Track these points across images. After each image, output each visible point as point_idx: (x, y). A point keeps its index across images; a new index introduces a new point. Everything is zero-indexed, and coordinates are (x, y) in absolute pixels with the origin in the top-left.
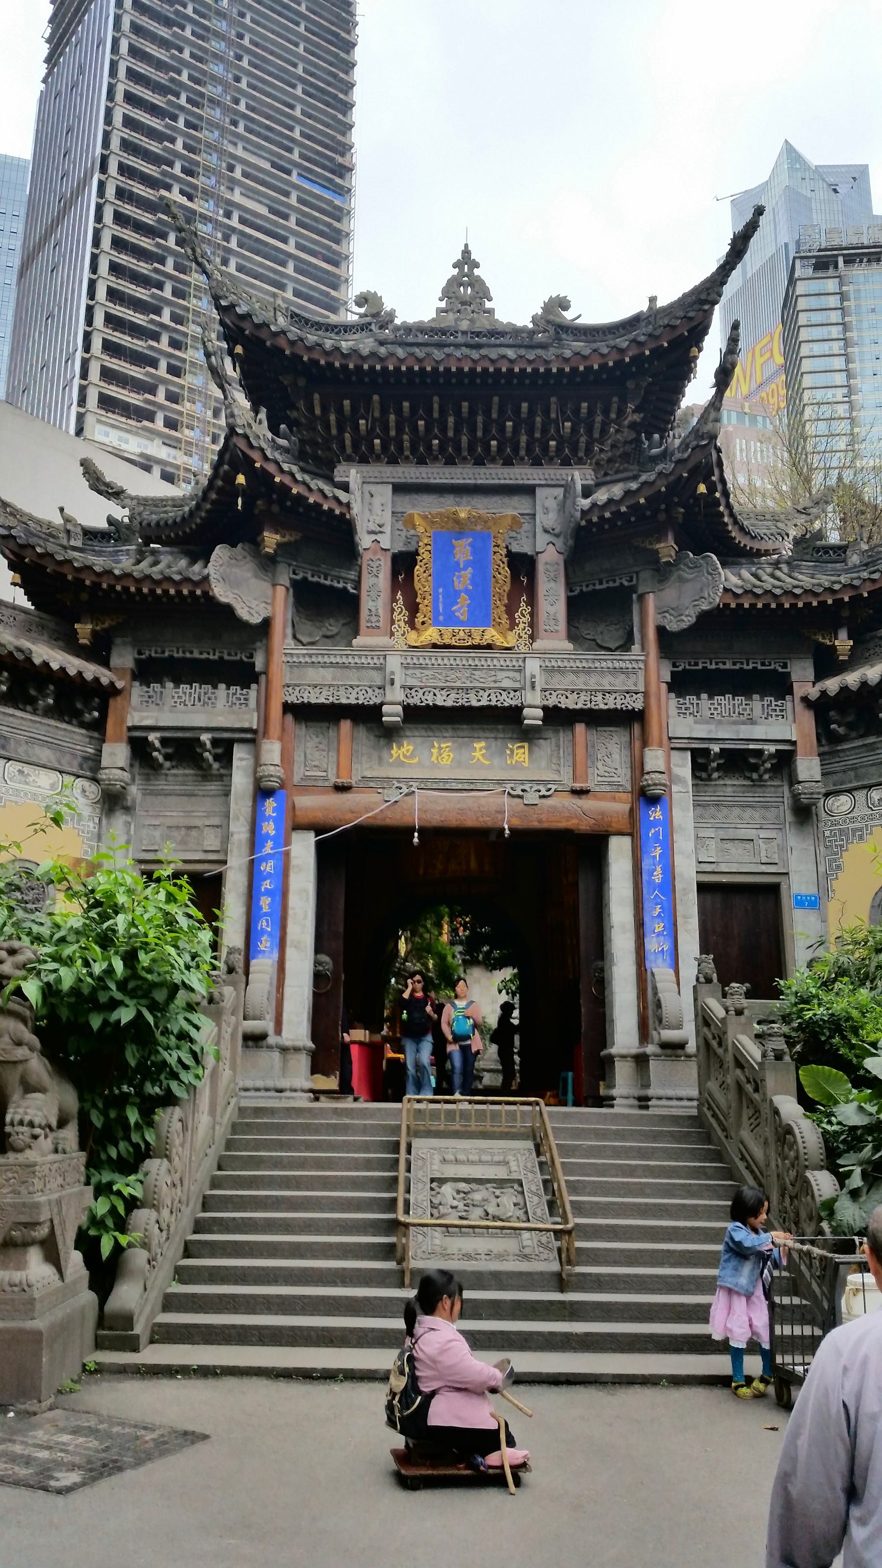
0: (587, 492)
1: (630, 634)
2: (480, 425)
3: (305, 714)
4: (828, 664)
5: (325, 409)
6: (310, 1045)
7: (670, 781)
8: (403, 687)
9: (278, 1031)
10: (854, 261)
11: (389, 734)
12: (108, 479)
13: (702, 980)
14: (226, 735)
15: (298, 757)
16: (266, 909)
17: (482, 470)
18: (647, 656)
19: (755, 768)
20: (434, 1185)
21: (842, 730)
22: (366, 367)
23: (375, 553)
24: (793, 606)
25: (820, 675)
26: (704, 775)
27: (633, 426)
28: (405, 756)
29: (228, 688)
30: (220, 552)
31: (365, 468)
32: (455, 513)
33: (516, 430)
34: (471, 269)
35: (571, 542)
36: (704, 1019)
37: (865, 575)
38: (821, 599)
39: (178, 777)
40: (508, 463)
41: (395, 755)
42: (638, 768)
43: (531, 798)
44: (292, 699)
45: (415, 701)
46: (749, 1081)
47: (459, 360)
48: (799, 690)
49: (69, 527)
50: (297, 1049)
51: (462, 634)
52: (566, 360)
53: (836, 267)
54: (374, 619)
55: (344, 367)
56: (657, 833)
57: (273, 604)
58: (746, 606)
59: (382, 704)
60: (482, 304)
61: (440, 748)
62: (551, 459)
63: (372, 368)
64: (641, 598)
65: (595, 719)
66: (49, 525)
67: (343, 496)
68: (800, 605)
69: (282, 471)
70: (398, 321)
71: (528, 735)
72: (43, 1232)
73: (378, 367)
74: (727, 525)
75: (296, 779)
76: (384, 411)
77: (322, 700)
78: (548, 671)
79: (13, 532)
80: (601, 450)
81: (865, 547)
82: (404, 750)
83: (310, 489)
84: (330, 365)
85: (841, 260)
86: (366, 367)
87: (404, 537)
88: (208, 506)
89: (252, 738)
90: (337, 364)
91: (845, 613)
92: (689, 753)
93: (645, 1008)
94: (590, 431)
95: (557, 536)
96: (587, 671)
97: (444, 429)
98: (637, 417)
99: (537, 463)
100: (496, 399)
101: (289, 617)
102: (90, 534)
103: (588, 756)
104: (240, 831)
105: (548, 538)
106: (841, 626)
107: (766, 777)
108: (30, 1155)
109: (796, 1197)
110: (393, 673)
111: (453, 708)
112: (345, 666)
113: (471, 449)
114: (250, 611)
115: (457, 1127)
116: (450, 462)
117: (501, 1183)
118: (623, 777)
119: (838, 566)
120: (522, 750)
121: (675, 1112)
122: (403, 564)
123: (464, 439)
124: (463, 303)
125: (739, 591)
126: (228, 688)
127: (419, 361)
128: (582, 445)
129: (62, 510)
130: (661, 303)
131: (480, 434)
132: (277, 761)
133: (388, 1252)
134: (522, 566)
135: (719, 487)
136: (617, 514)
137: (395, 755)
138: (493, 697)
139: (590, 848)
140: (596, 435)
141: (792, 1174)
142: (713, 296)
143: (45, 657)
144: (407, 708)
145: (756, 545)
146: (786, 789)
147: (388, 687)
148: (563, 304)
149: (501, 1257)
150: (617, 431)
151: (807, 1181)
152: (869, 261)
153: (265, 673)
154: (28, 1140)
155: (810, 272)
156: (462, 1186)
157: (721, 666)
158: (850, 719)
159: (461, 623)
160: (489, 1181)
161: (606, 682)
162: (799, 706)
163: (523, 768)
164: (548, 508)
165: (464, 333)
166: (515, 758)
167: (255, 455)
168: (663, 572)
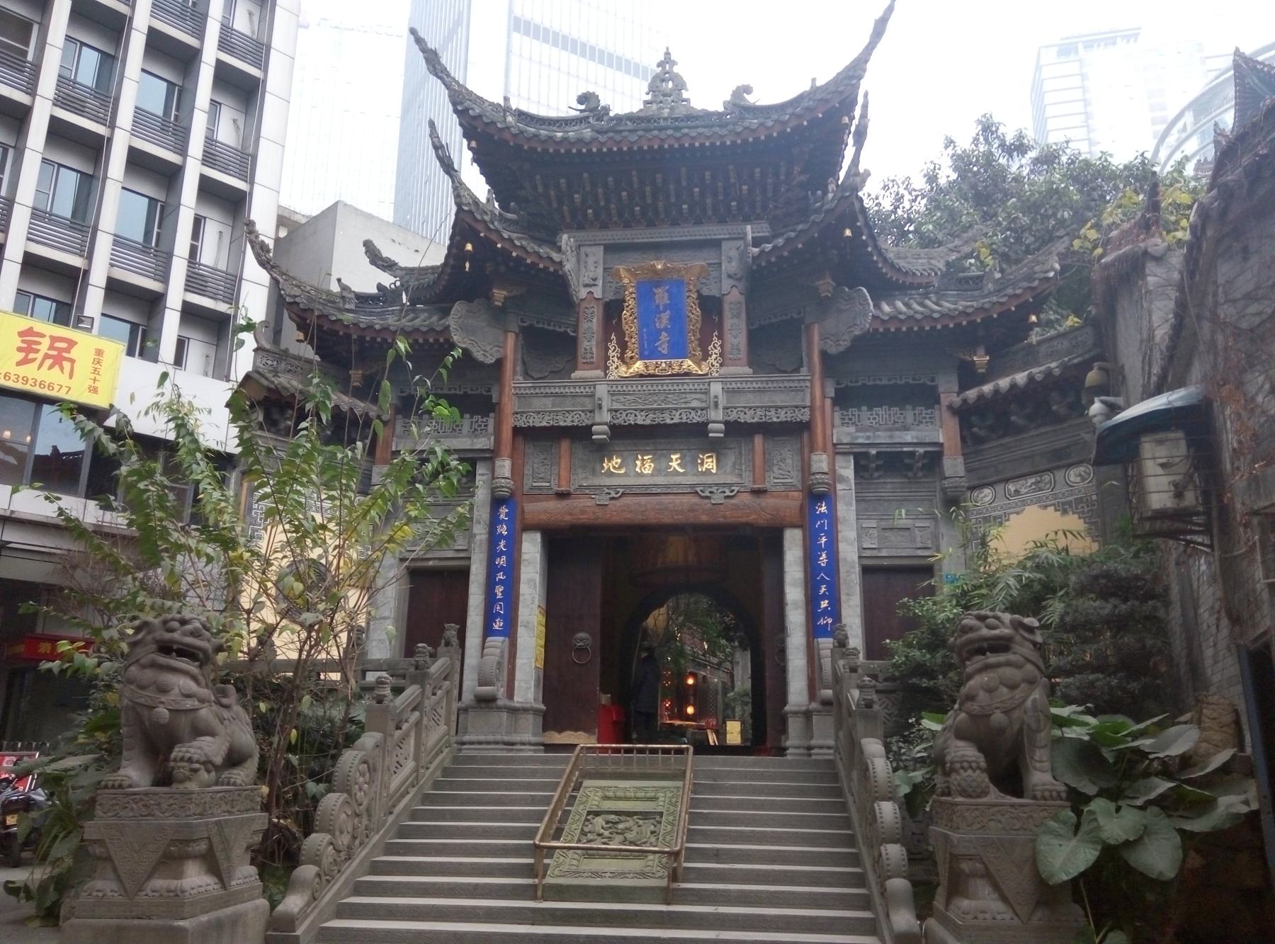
0: (757, 242)
3: (524, 434)
4: (969, 377)
6: (543, 707)
8: (610, 410)
9: (510, 695)
10: (1092, 46)
11: (602, 450)
12: (384, 255)
14: (470, 455)
15: (528, 471)
16: (499, 596)
17: (678, 230)
18: (813, 376)
19: (910, 467)
22: (574, 151)
25: (964, 387)
26: (866, 475)
30: (458, 308)
32: (653, 266)
33: (702, 194)
34: (671, 67)
38: (957, 321)
40: (698, 222)
42: (806, 469)
43: (718, 498)
44: (521, 424)
45: (620, 421)
47: (650, 140)
48: (945, 400)
49: (345, 294)
50: (525, 710)
52: (738, 134)
53: (1077, 52)
54: (588, 356)
57: (504, 347)
60: (680, 94)
63: (579, 151)
64: (808, 327)
65: (771, 431)
68: (939, 327)
69: (503, 238)
71: (715, 447)
72: (203, 847)
73: (584, 150)
75: (526, 488)
77: (544, 424)
78: (726, 391)
79: (297, 300)
80: (776, 207)
81: (998, 275)
84: (545, 151)
85: (1080, 46)
86: (574, 151)
89: (490, 456)
90: (551, 150)
92: (852, 458)
95: (739, 280)
96: (761, 391)
97: (643, 197)
99: (722, 221)
101: (519, 357)
102: (363, 299)
103: (765, 461)
104: (480, 532)
105: (732, 282)
108: (192, 786)
111: (651, 426)
114: (485, 354)
115: (622, 769)
117: (645, 815)
118: (795, 479)
119: (976, 293)
122: (613, 310)
124: (664, 95)
127: (618, 143)
130: (818, 84)
131: (673, 199)
132: (508, 474)
133: (529, 871)
134: (711, 307)
138: (684, 417)
140: (770, 195)
142: (859, 72)
144: (613, 427)
148: (747, 89)
149: (623, 875)
152: (1106, 45)
153: (499, 404)
154: (187, 773)
156: (612, 817)
157: (878, 382)
158: (989, 423)
160: (635, 813)
161: (779, 399)
162: (946, 415)
164: (731, 260)
165: (665, 119)
167: (480, 227)
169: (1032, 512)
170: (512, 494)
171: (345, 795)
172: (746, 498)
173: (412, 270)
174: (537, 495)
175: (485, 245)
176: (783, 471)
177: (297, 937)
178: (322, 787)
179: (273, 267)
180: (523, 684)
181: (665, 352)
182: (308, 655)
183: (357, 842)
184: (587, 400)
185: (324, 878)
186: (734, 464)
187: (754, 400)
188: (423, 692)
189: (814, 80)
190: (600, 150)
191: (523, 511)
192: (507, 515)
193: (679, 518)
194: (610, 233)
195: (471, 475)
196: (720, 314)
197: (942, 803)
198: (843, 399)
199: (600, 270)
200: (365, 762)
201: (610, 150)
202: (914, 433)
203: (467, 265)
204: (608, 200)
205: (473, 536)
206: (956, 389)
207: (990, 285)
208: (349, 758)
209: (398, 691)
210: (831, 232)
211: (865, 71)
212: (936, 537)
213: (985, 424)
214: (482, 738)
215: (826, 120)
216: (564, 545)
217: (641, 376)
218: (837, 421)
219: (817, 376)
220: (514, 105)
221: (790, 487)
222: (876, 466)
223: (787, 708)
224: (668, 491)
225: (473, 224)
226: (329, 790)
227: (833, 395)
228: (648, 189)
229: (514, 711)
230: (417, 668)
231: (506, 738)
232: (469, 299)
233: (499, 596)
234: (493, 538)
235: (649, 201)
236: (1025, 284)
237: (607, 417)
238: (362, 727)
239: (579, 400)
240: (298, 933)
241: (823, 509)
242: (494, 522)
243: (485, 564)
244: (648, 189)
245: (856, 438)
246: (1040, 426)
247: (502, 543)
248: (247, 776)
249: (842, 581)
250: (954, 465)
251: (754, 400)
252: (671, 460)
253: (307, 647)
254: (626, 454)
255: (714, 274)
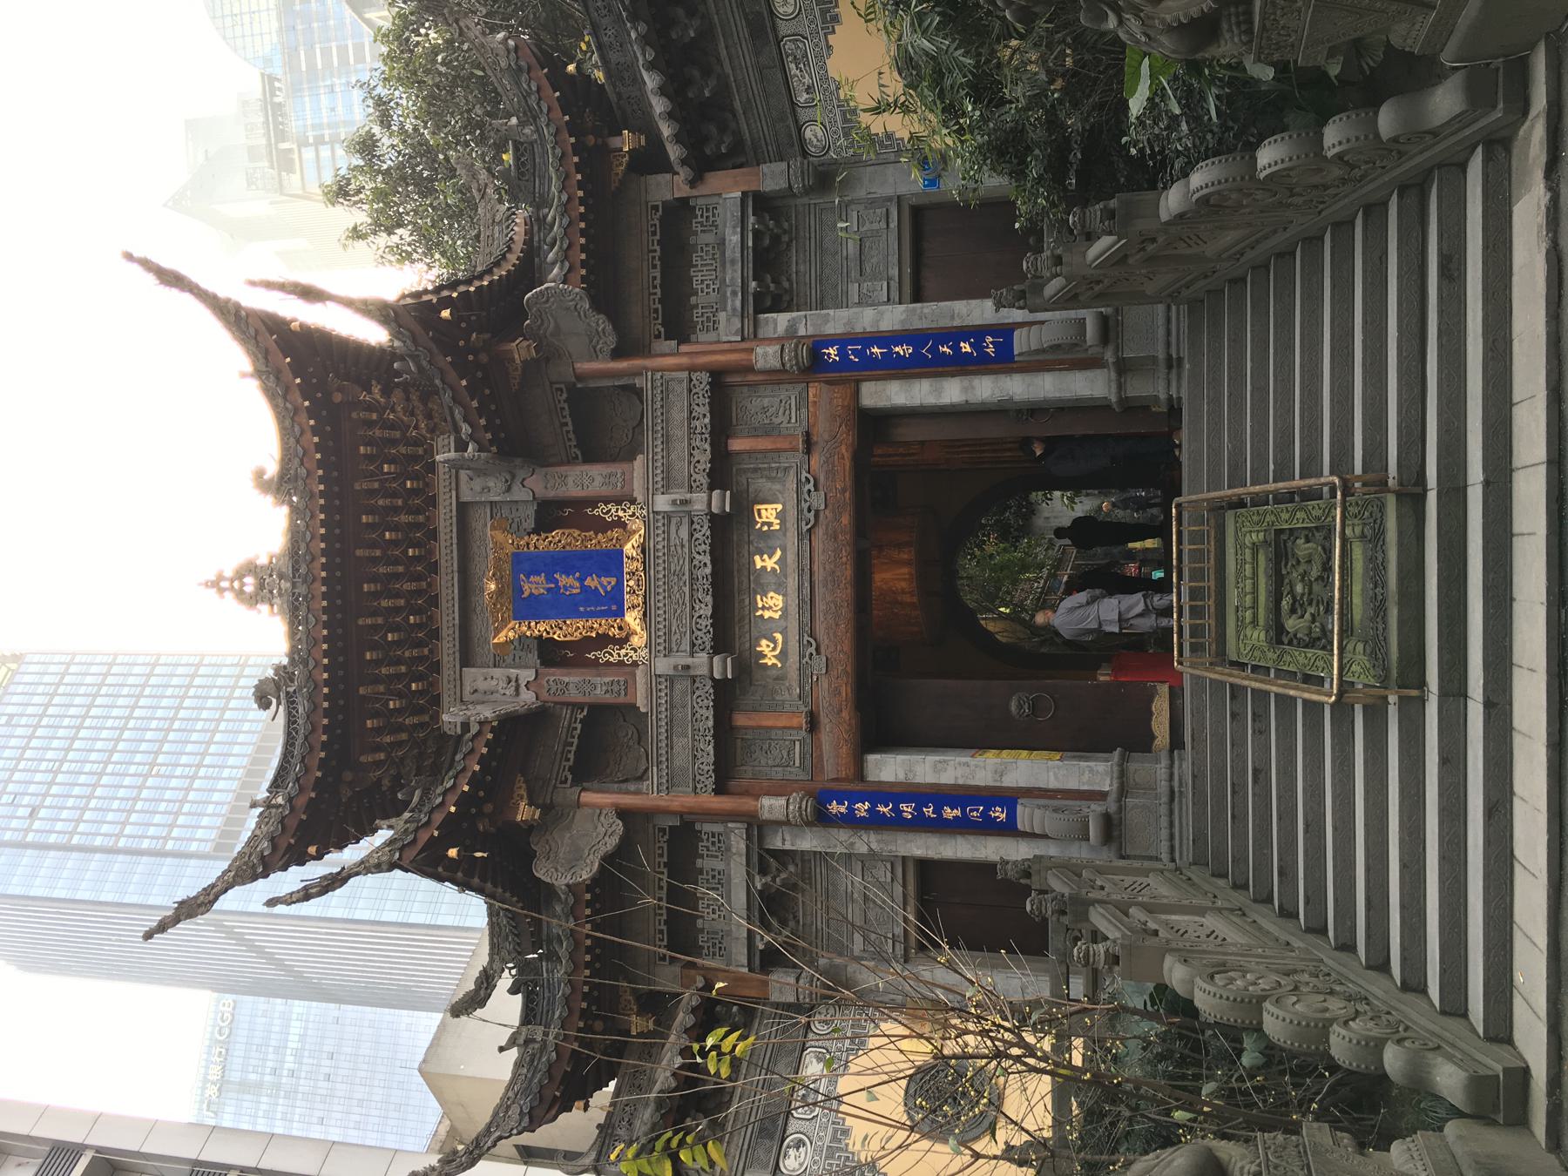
0: (461, 446)
1: (623, 387)
2: (390, 569)
5: (378, 748)
6: (1117, 753)
7: (792, 338)
9: (1102, 796)
10: (283, 131)
11: (747, 666)
13: (1022, 303)
15: (778, 773)
16: (957, 812)
18: (647, 369)
19: (776, 239)
20: (1286, 640)
21: (728, 139)
23: (542, 686)
24: (582, 201)
26: (786, 298)
27: (386, 392)
28: (774, 649)
29: (702, 856)
30: (542, 872)
31: (445, 699)
33: (395, 528)
35: (518, 461)
36: (1069, 300)
37: (543, 120)
39: (809, 906)
40: (433, 535)
41: (774, 661)
42: (777, 377)
43: (818, 501)
44: (710, 783)
45: (708, 639)
46: (1143, 249)
48: (683, 190)
49: (521, 1041)
50: (1122, 774)
51: (631, 583)
55: (326, 729)
56: (854, 352)
58: (583, 256)
59: (713, 679)
61: (763, 608)
62: (427, 485)
63: (326, 697)
64: (580, 377)
65: (721, 429)
66: (518, 1064)
67: (474, 729)
68: (580, 193)
69: (442, 804)
70: (285, 661)
71: (743, 510)
73: (326, 690)
74: (491, 282)
76: (377, 680)
77: (710, 749)
80: (416, 427)
81: (514, 120)
82: (767, 651)
83: (464, 769)
87: (523, 654)
88: (489, 885)
89: (757, 828)
91: (591, 140)
93: (1061, 362)
94: (394, 442)
95: (513, 477)
96: (667, 440)
97: (397, 610)
98: (376, 390)
99: (432, 502)
100: (359, 553)
102: (528, 1016)
104: (867, 842)
105: (516, 487)
106: (606, 144)
107: (786, 225)
109: (1291, 190)
110: (675, 668)
112: (670, 723)
113: (418, 578)
114: (608, 835)
116: (434, 601)
118: (790, 394)
120: (763, 513)
121: (1185, 325)
122: (551, 653)
123: (407, 586)
125: (567, 264)
126: (702, 856)
128: (410, 450)
129: (501, 1049)
132: (782, 801)
134: (550, 515)
135: (445, 293)
136: (480, 411)
137: (774, 661)
139: (874, 427)
141: (1259, 195)
143: (668, 1074)
144: (716, 650)
145: (518, 246)
146: (799, 201)
147: (692, 673)
148: (259, 474)
150: (393, 410)
151: (1270, 177)
153: (681, 814)
155: (295, 178)
156: (1285, 604)
157: (658, 282)
159: (620, 583)
161: (679, 415)
163: (783, 510)
164: (483, 489)
165: (294, 585)
166: (772, 519)
167: (424, 837)
168: (548, 354)
169: (837, 67)
170: (809, 794)
171: (1267, 1005)
172: (816, 460)
173: (492, 945)
174: (813, 762)
175: (452, 830)
176: (782, 411)
177: (1505, 1070)
178: (1248, 1042)
179: (478, 1146)
180: (1087, 776)
181: (613, 581)
182: (1045, 1058)
183: (1338, 988)
184: (678, 687)
185: (1402, 1034)
186: (769, 478)
187: (680, 448)
188: (1101, 902)
189: (244, 375)
190: (326, 668)
191: (833, 780)
192: (840, 803)
193: (846, 555)
194: (446, 659)
195: (783, 856)
196: (562, 503)
197: (1263, 28)
198: (679, 327)
199: (497, 672)
200: (1212, 977)
201: (326, 654)
202: (728, 231)
203: (478, 854)
204: (399, 662)
205: (872, 854)
206: (668, 176)
207: (527, 131)
208: (1207, 1000)
209: (1096, 937)
210: (444, 337)
211: (228, 301)
212: (872, 203)
213: (712, 137)
214: (1164, 834)
215: (297, 363)
216: (881, 729)
217: (645, 614)
218: (712, 336)
219: (648, 363)
220: (262, 794)
221: (802, 401)
222: (772, 282)
223: (1114, 399)
224: (807, 572)
225: (420, 844)
226: (1258, 1029)
227: (674, 343)
228: (384, 603)
229: (1123, 791)
230: (1063, 913)
231: (1165, 799)
232: (531, 855)
233: (957, 812)
234: (875, 822)
235: (402, 602)
236: (524, 77)
237: (702, 658)
238: (1162, 989)
239: (677, 699)
240: (1499, 1069)
241: (832, 351)
242: (850, 820)
243: (911, 836)
244: (384, 603)
245: (734, 310)
246: (719, 60)
247: (882, 809)
248: (1243, 1157)
249: (934, 325)
250: (772, 177)
251: (680, 448)
252: (764, 568)
253: (1031, 1061)
254: (754, 633)
255: (505, 512)
